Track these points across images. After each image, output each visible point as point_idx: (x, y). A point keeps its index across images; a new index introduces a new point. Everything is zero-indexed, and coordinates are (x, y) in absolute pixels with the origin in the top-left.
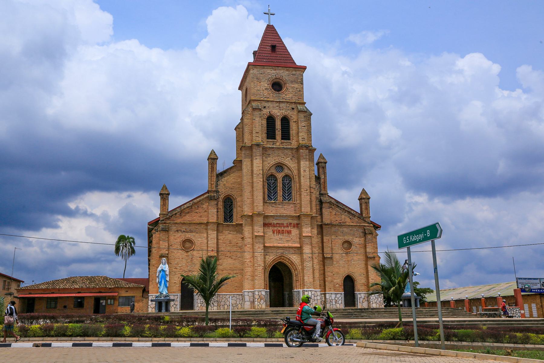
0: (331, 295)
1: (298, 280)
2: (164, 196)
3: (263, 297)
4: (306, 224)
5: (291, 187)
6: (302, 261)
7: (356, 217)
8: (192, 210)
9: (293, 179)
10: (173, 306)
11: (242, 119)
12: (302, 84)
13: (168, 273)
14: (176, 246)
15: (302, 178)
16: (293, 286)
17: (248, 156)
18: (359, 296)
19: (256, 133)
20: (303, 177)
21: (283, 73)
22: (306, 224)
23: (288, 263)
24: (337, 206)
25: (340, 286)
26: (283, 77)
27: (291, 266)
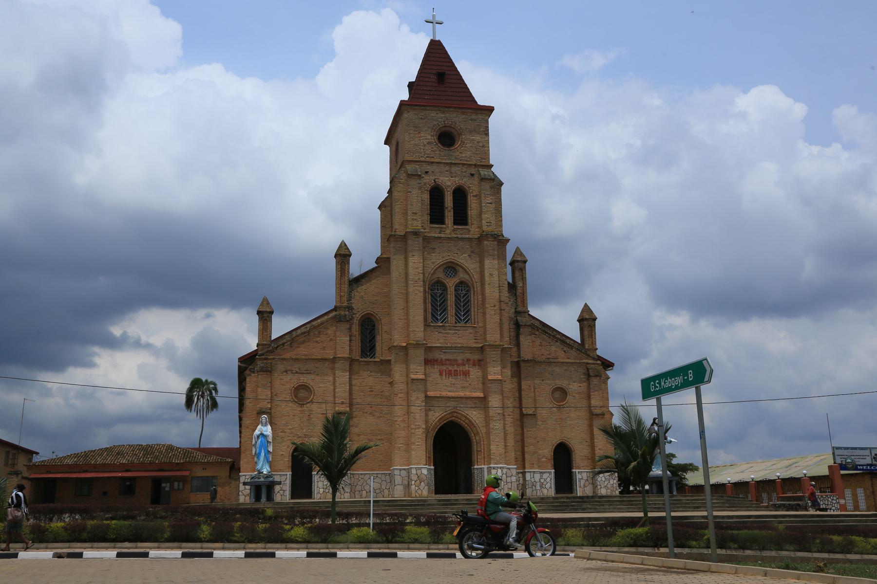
1: (481, 451)
2: (265, 315)
3: (424, 478)
4: (493, 361)
6: (487, 420)
7: (574, 350)
8: (309, 337)
10: (278, 492)
12: (487, 134)
15: (486, 287)
18: (578, 476)
19: (413, 213)
20: (489, 284)
22: (493, 361)
23: (464, 423)
25: (549, 460)
26: (456, 123)
27: (468, 428)
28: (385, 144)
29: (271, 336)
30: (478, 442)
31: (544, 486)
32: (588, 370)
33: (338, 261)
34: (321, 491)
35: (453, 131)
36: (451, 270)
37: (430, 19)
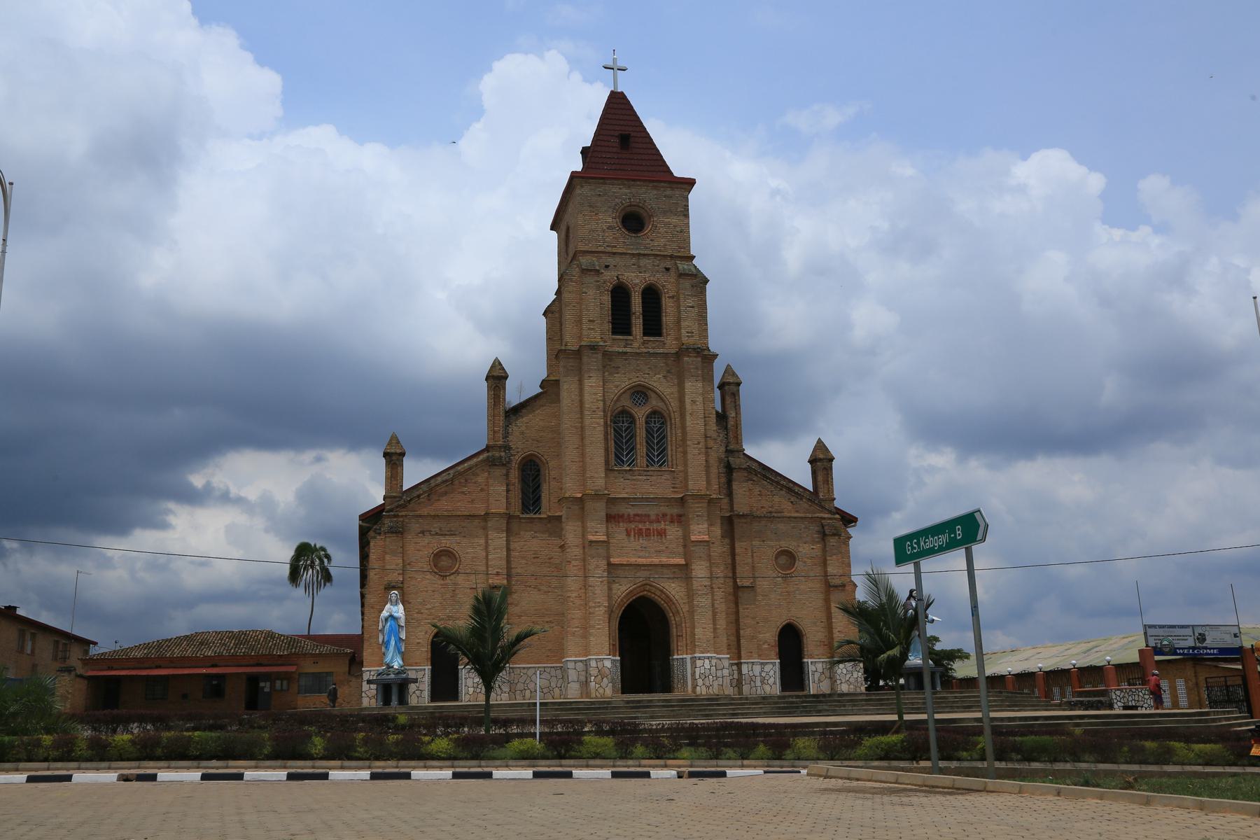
0: (752, 667)
2: (394, 458)
3: (607, 672)
4: (697, 516)
6: (690, 595)
7: (804, 500)
9: (668, 419)
10: (414, 692)
12: (687, 216)
18: (812, 668)
19: (590, 321)
22: (697, 516)
23: (660, 600)
24: (764, 476)
25: (772, 646)
27: (665, 605)
28: (551, 229)
30: (678, 624)
31: (766, 681)
34: (471, 690)
36: (641, 396)
37: (610, 64)
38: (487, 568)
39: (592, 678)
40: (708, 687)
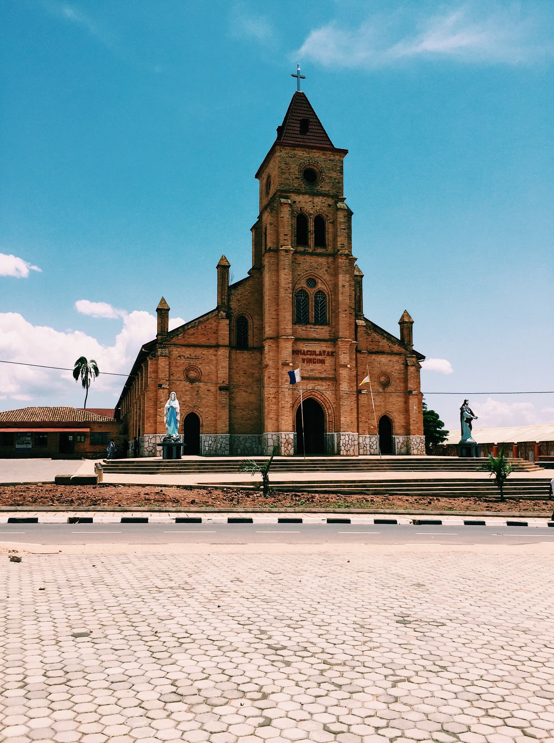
1: (332, 421)
2: (163, 312)
3: (291, 441)
4: (344, 353)
5: (324, 306)
6: (338, 398)
9: (327, 296)
11: (260, 217)
12: (342, 173)
13: (178, 410)
14: (179, 375)
16: (325, 428)
17: (273, 264)
18: (397, 440)
19: (285, 235)
20: (341, 293)
21: (318, 157)
22: (344, 353)
26: (318, 162)
28: (256, 178)
29: (168, 329)
32: (406, 361)
33: (219, 271)
34: (207, 448)
35: (315, 169)
36: (312, 281)
37: (296, 73)
38: (217, 378)
39: (283, 444)
40: (347, 451)
